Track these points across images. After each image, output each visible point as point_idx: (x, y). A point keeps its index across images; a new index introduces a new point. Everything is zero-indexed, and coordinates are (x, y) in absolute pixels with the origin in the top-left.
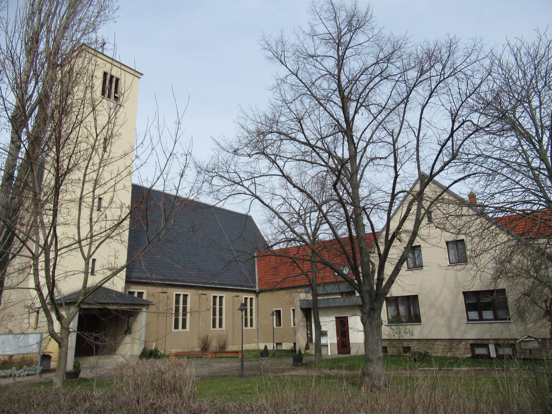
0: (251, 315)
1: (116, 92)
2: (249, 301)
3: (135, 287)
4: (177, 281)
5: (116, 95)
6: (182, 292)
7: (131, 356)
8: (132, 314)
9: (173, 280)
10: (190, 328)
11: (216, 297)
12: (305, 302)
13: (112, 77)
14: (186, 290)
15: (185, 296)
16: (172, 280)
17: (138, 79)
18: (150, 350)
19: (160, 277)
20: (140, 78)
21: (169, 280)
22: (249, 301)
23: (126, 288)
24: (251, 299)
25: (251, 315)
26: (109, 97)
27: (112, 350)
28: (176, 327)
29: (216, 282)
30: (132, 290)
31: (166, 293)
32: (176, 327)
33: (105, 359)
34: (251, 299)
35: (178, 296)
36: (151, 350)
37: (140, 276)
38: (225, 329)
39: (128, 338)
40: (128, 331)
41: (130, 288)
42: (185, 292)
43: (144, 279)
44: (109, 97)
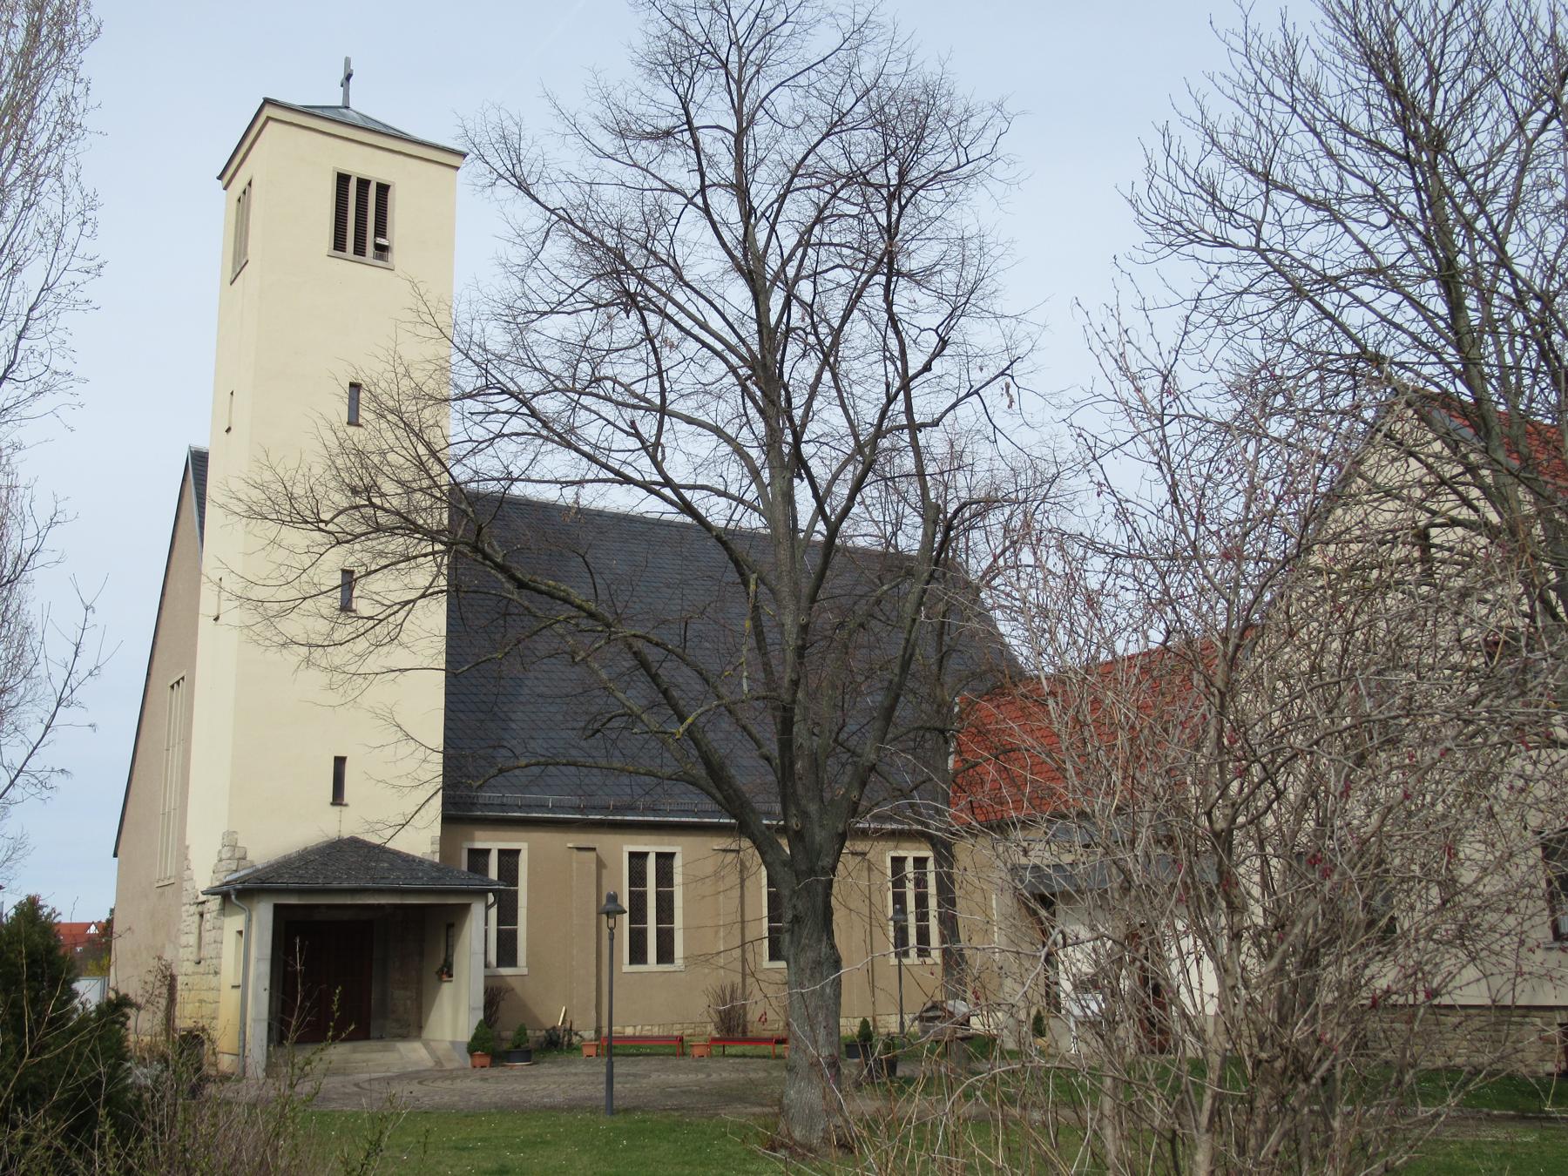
0: (922, 916)
1: (381, 230)
2: (909, 866)
3: (907, 845)
4: (631, 809)
5: (381, 241)
6: (651, 846)
7: (453, 1043)
8: (449, 920)
9: (617, 810)
10: (528, 965)
11: (643, 856)
12: (768, 859)
13: (363, 184)
14: (666, 839)
15: (665, 859)
16: (615, 807)
17: (452, 171)
18: (549, 1026)
19: (575, 800)
20: (457, 168)
21: (604, 809)
22: (909, 866)
23: (446, 841)
24: (920, 862)
25: (922, 916)
26: (360, 250)
27: (412, 1026)
28: (638, 955)
29: (550, 800)
30: (479, 845)
31: (594, 849)
32: (638, 955)
33: (372, 1051)
34: (920, 862)
35: (638, 858)
36: (554, 1028)
37: (505, 800)
38: (525, 971)
39: (447, 989)
40: (446, 971)
41: (472, 840)
42: (919, 849)
43: (520, 808)
44: (360, 250)
